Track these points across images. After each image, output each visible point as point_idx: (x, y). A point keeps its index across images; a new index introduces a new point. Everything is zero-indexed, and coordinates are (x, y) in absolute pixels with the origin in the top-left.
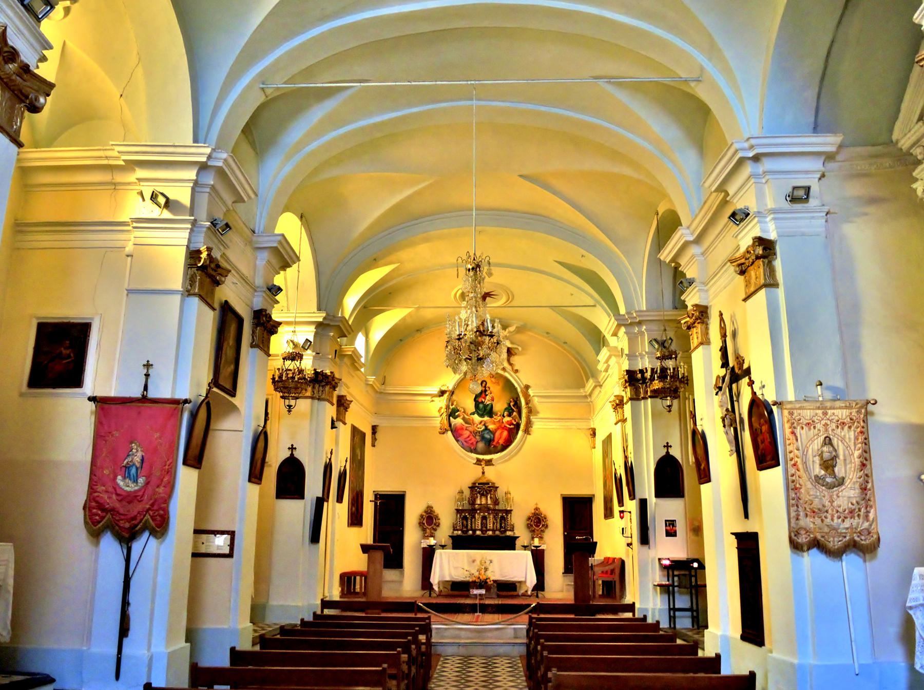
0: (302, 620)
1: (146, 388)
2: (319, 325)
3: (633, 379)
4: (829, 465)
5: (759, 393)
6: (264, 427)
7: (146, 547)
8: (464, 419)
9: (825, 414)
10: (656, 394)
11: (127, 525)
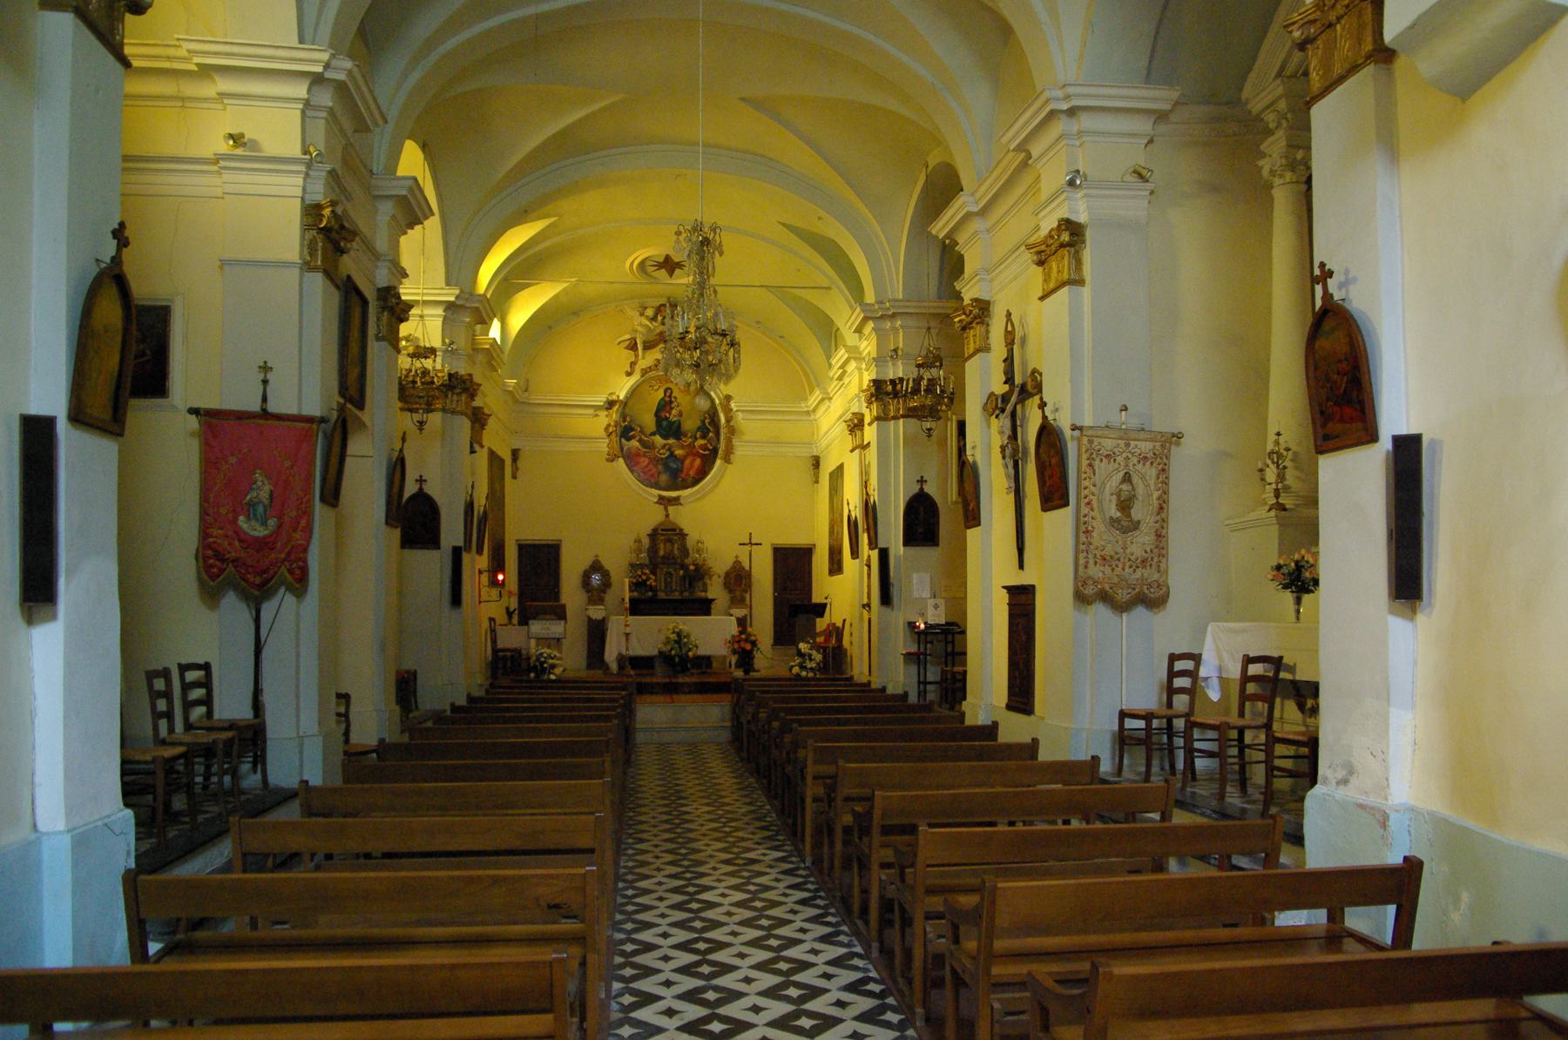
0: (452, 705)
1: (264, 399)
2: (450, 307)
3: (880, 391)
4: (1125, 505)
5: (1050, 417)
6: (401, 450)
7: (282, 609)
8: (640, 441)
9: (1127, 445)
10: (911, 413)
11: (258, 580)
